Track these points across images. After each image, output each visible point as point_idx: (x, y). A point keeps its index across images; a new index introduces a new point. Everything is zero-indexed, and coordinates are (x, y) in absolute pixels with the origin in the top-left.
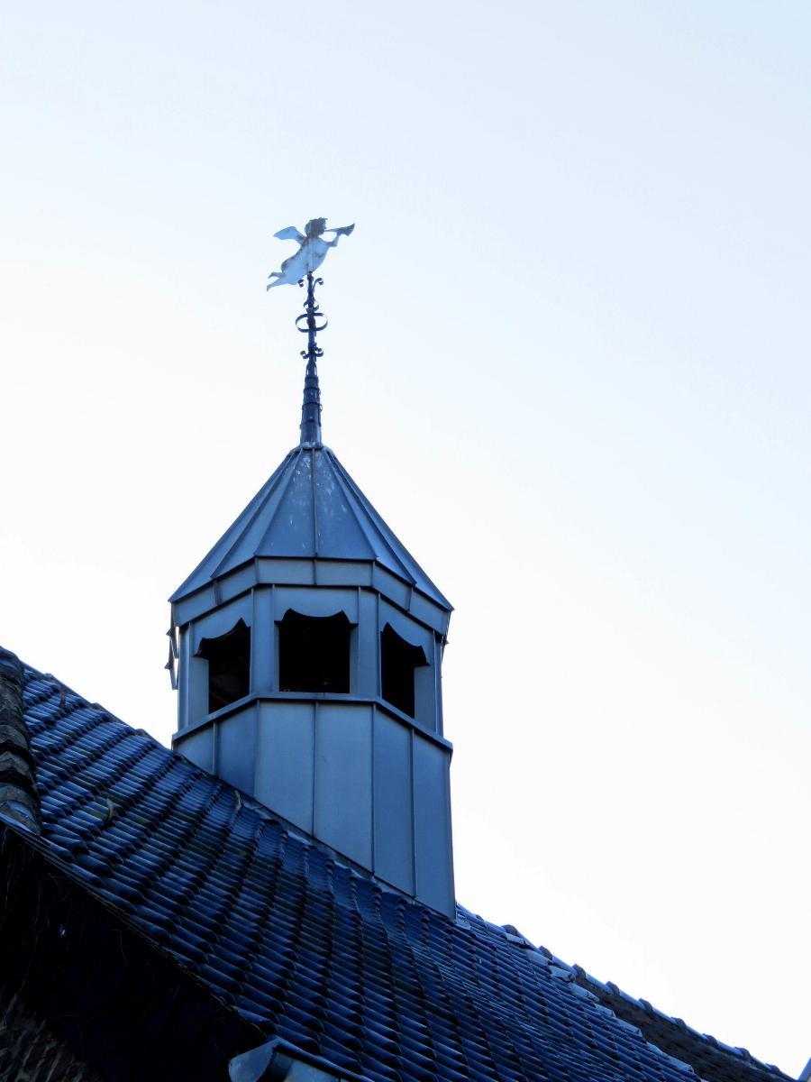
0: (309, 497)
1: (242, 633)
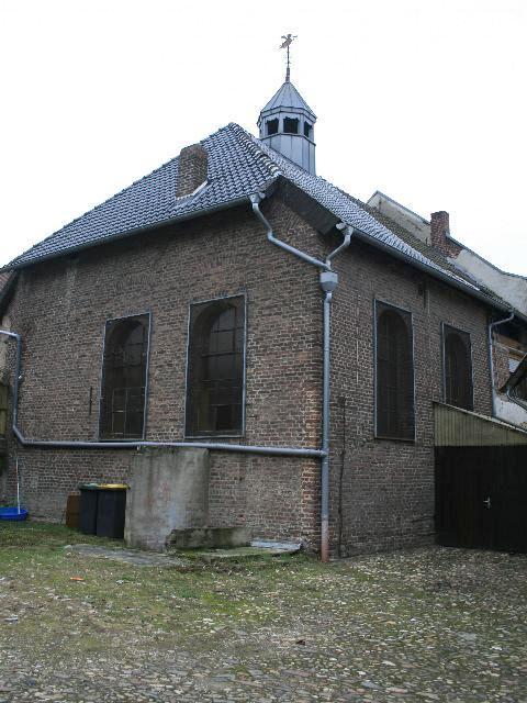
0: (116, 533)
1: (276, 121)
